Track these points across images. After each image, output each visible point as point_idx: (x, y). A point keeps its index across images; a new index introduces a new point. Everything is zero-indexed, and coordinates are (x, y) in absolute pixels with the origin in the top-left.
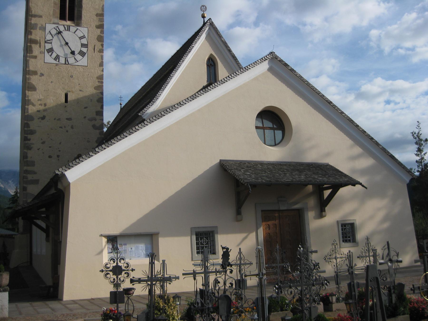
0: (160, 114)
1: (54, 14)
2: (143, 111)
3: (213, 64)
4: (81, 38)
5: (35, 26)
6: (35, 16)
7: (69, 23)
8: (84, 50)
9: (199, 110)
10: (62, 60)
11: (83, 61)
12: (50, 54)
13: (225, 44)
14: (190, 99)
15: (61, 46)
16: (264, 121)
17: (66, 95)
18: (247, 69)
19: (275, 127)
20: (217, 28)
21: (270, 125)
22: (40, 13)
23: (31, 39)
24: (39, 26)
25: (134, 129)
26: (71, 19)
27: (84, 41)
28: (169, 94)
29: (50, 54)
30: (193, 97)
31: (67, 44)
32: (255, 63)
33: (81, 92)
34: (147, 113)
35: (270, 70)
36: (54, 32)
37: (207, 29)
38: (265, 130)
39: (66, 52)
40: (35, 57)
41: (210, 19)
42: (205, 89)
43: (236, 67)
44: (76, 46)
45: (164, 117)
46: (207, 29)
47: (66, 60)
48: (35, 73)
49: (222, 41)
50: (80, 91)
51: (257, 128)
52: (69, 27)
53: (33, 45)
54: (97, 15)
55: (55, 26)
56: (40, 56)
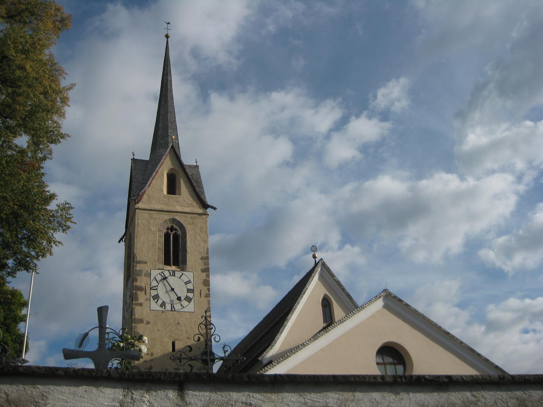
0: (286, 355)
1: (158, 260)
2: (263, 355)
3: (327, 304)
4: (186, 283)
5: (140, 273)
6: (140, 262)
7: (173, 268)
8: (190, 295)
9: (321, 350)
10: (168, 307)
11: (190, 307)
12: (156, 300)
13: (348, 296)
14: (312, 339)
15: (167, 292)
16: (384, 357)
17: (173, 344)
18: (363, 307)
19: (395, 361)
20: (340, 283)
21: (390, 360)
22: (145, 259)
23: (136, 286)
24: (144, 272)
25: (263, 370)
26: (176, 264)
27: (190, 286)
28: (287, 337)
29: (156, 300)
30: (315, 337)
31: (173, 289)
32: (370, 301)
33: (188, 340)
34: (266, 358)
35: (386, 306)
36: (159, 278)
37: (319, 269)
38: (387, 366)
39: (172, 299)
40: (141, 305)
41: (321, 259)
42: (325, 329)
43: (351, 307)
44: (182, 292)
45: (290, 358)
46: (319, 269)
47: (172, 306)
48: (141, 321)
49: (335, 280)
50: (188, 338)
51: (378, 364)
52: (174, 272)
53: (139, 292)
54: (202, 258)
55: (160, 271)
56: (146, 304)
